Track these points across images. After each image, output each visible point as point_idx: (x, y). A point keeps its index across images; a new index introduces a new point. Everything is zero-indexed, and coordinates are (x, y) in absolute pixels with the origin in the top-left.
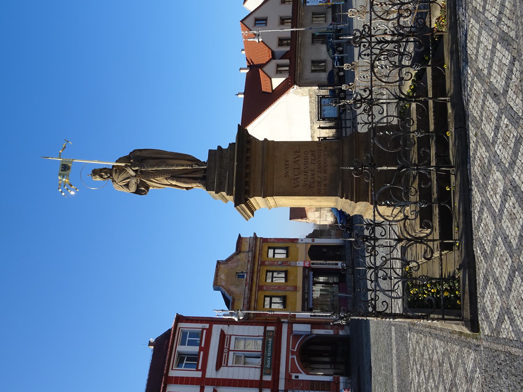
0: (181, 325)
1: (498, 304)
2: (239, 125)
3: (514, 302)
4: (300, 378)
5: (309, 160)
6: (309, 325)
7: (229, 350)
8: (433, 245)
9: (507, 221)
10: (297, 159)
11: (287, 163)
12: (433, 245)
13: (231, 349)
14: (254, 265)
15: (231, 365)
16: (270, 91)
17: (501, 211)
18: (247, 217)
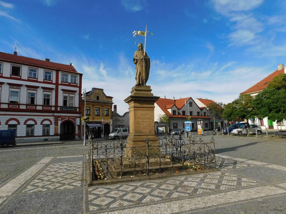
0: (79, 76)
1: (100, 193)
2: (160, 97)
3: (102, 199)
6: (79, 124)
7: (69, 94)
9: (132, 195)
11: (146, 115)
13: (70, 95)
14: (102, 103)
15: (10, 90)
16: (166, 108)
17: (135, 193)
18: (125, 100)
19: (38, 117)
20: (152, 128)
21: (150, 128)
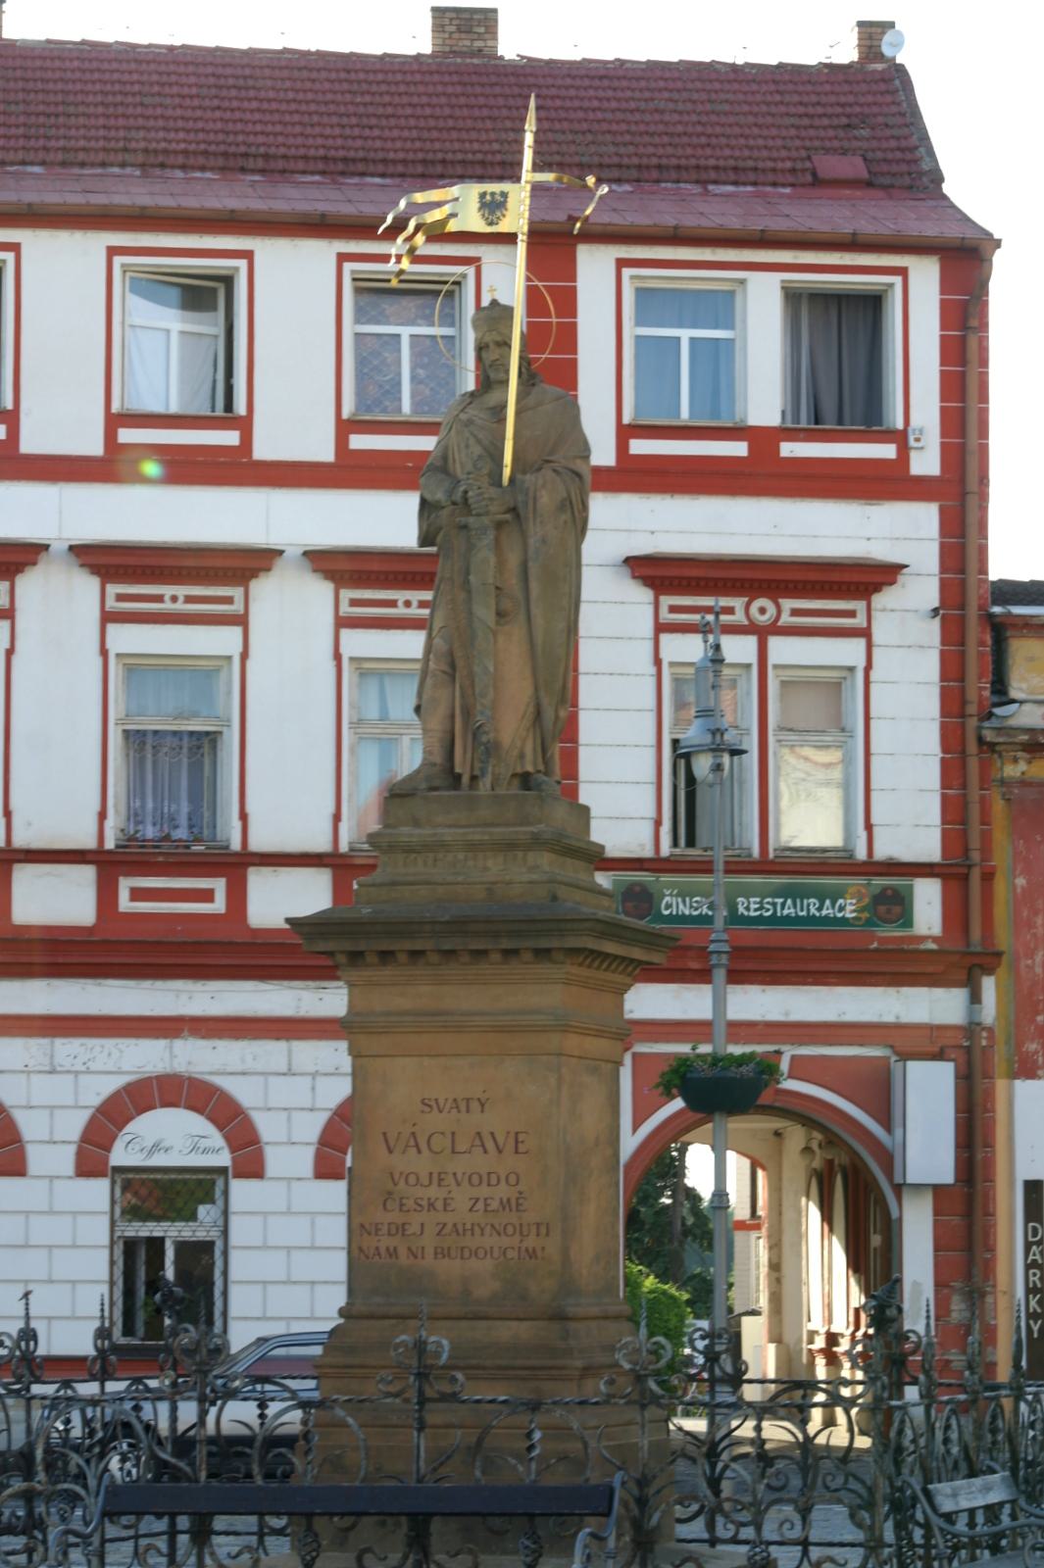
5: (484, 1191)
7: (764, 633)
10: (490, 1145)
11: (475, 1105)
19: (271, 1052)
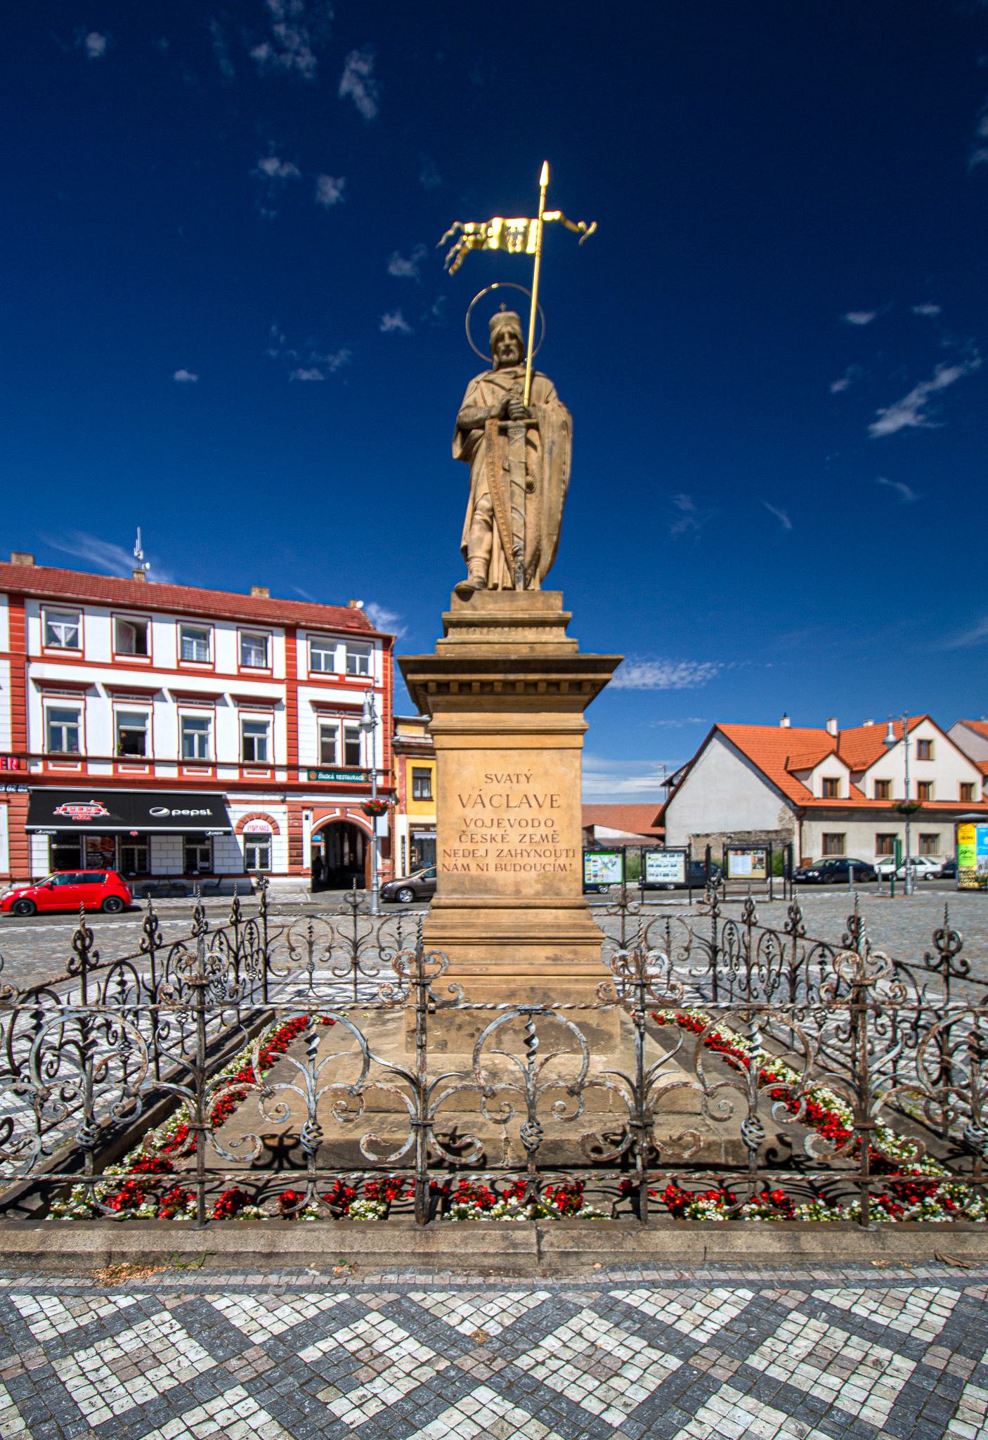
4: (305, 822)
5: (530, 830)
6: (385, 834)
8: (908, 832)
10: (533, 803)
11: (523, 779)
12: (908, 832)
20: (562, 861)
21: (544, 861)
